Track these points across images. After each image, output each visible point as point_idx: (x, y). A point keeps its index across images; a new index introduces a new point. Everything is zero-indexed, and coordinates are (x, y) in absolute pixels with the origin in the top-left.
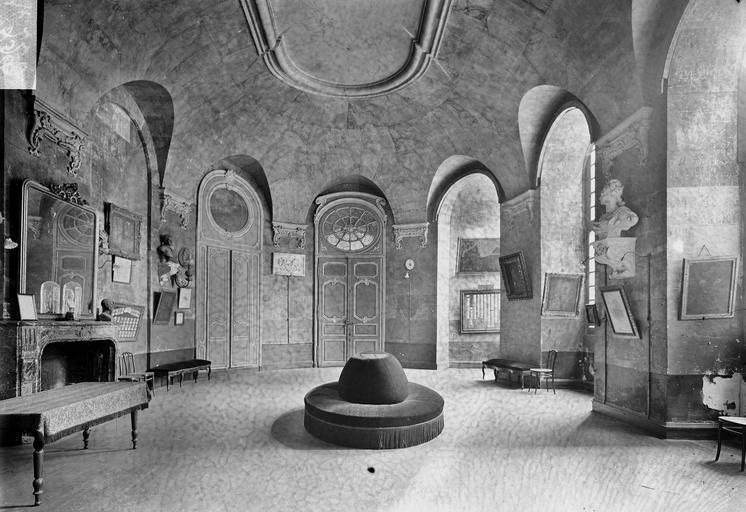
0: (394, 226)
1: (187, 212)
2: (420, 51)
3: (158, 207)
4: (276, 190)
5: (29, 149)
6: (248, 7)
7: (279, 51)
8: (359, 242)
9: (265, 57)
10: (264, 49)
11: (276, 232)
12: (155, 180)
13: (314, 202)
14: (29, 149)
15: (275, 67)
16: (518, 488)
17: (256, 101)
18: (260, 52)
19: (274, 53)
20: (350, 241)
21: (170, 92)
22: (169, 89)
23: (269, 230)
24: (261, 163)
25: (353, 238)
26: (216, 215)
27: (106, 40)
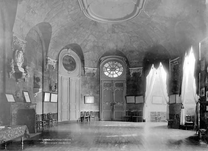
0: (130, 68)
1: (54, 65)
2: (138, 8)
3: (46, 63)
4: (86, 55)
5: (12, 49)
6: (82, 6)
7: (88, 9)
8: (116, 74)
9: (84, 11)
10: (83, 8)
11: (86, 71)
12: (45, 54)
13: (100, 59)
14: (12, 49)
15: (87, 14)
16: (57, 10)
17: (80, 25)
18: (82, 10)
19: (87, 10)
20: (116, 73)
21: (51, 24)
22: (51, 24)
23: (83, 70)
24: (81, 46)
25: (114, 73)
26: (65, 66)
27: (33, 12)
